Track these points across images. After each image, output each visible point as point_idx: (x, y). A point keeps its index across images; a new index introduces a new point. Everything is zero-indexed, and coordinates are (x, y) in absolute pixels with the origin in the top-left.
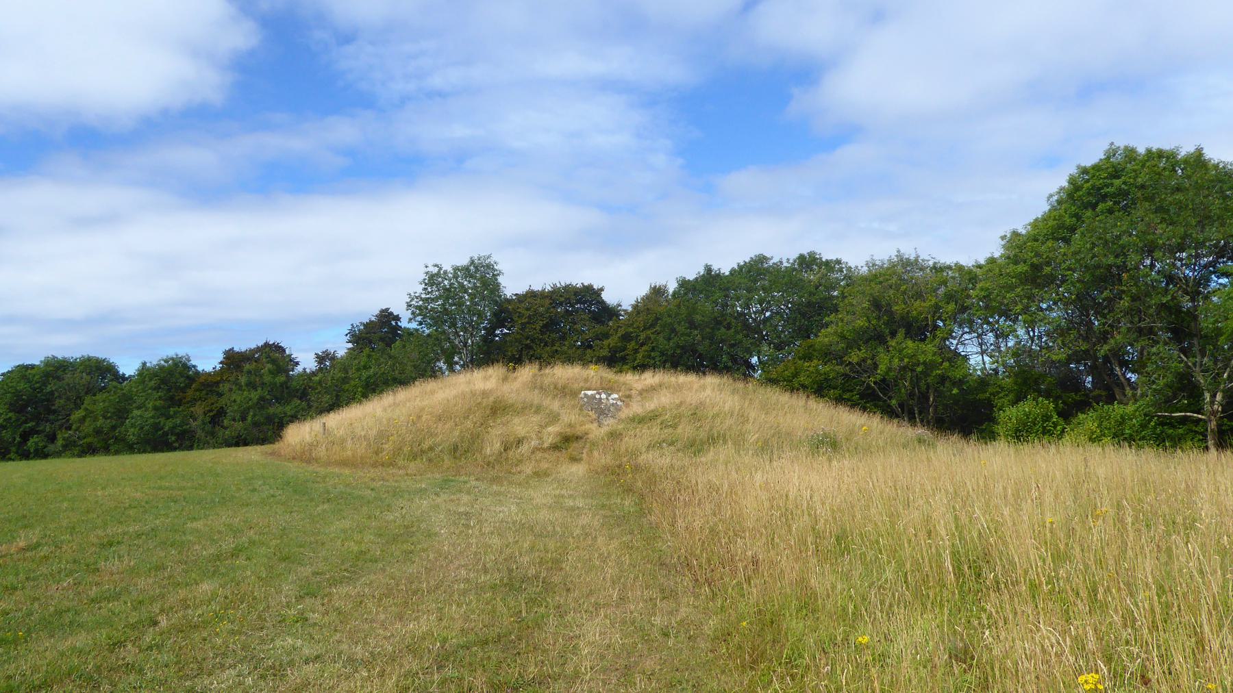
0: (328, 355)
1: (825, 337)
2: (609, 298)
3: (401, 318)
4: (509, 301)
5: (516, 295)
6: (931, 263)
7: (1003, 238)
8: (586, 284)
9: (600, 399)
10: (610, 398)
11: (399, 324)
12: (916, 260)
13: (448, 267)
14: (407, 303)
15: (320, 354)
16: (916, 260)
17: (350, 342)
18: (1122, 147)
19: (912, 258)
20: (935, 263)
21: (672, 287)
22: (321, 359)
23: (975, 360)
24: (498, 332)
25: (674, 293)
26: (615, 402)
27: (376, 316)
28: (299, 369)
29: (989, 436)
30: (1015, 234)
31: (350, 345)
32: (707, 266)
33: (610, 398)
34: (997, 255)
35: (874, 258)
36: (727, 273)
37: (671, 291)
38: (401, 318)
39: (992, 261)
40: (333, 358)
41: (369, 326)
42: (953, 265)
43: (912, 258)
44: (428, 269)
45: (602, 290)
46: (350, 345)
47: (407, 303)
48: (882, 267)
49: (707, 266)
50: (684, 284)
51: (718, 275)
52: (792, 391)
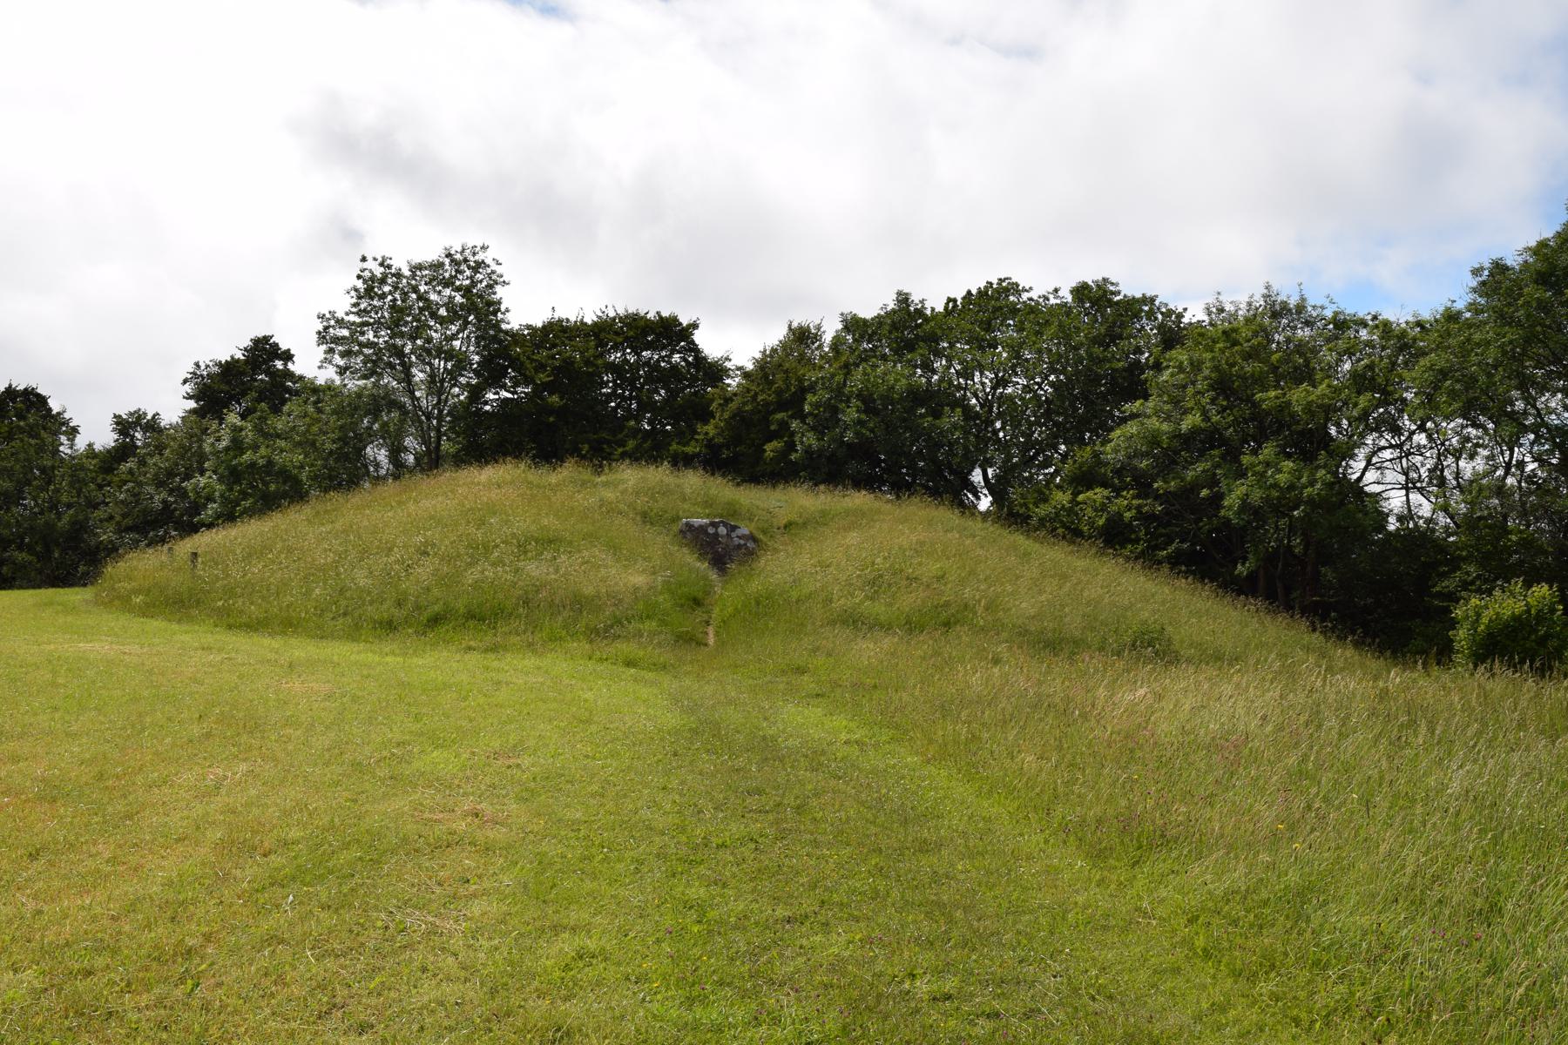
0: (139, 418)
1: (1119, 443)
2: (710, 343)
3: (293, 356)
4: (515, 336)
5: (529, 327)
6: (1329, 313)
7: (1476, 272)
8: (665, 314)
9: (716, 535)
10: (733, 535)
11: (290, 366)
12: (1301, 308)
13: (401, 263)
14: (319, 333)
15: (124, 417)
16: (1301, 308)
17: (189, 397)
18: (1487, 265)
19: (1293, 302)
20: (1336, 314)
21: (831, 330)
22: (124, 426)
23: (1395, 501)
24: (490, 396)
25: (837, 343)
26: (742, 542)
27: (246, 349)
28: (81, 443)
29: (1443, 653)
30: (1499, 268)
31: (192, 404)
32: (899, 293)
33: (733, 535)
34: (1460, 305)
35: (1221, 298)
36: (940, 308)
37: (828, 338)
38: (293, 356)
39: (1451, 316)
40: (152, 426)
41: (229, 370)
42: (1369, 317)
43: (1293, 302)
44: (365, 265)
45: (695, 326)
46: (192, 404)
47: (319, 333)
48: (1234, 315)
49: (899, 293)
50: (853, 324)
51: (920, 313)
52: (656, 461)
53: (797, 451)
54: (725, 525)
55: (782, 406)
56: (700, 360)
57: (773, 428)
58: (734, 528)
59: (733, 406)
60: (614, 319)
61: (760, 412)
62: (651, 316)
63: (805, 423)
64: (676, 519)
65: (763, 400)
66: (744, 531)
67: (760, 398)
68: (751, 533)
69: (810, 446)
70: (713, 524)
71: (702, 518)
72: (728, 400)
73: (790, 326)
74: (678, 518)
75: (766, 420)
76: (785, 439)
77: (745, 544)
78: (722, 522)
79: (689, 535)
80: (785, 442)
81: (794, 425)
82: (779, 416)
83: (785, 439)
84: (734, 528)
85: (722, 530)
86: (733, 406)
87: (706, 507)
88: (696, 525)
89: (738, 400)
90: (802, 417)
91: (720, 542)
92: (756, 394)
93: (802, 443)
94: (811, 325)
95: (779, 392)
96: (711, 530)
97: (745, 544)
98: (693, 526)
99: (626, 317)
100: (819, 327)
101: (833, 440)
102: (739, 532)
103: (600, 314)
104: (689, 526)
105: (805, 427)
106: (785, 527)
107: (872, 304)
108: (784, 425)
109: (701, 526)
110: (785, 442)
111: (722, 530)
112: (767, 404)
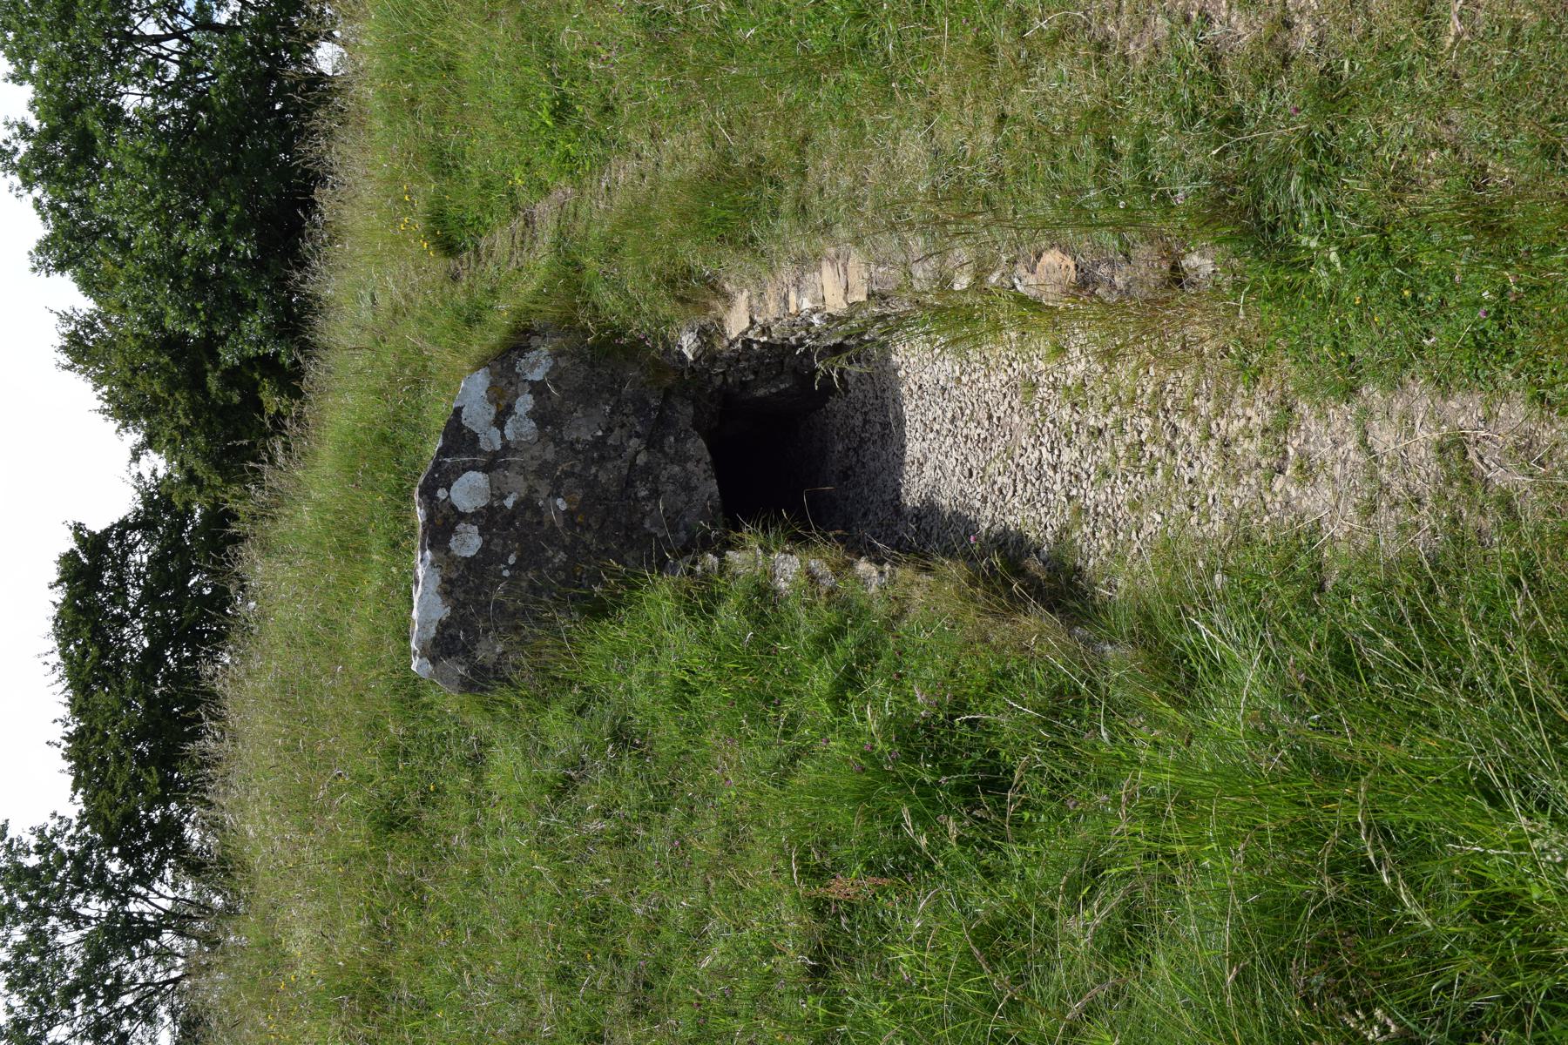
9: (488, 518)
10: (491, 440)
26: (525, 403)
33: (491, 440)
45: (78, 528)
53: (277, 354)
54: (442, 476)
55: (196, 382)
56: (144, 522)
57: (236, 399)
58: (458, 437)
59: (200, 468)
60: (63, 656)
61: (209, 422)
62: (59, 595)
63: (226, 337)
64: (409, 692)
65: (186, 415)
66: (473, 394)
67: (184, 421)
68: (482, 363)
69: (267, 328)
70: (441, 528)
71: (409, 579)
72: (191, 477)
73: (69, 368)
74: (409, 692)
75: (225, 412)
76: (257, 376)
77: (538, 389)
78: (428, 491)
79: (489, 650)
80: (263, 376)
81: (228, 357)
82: (213, 383)
83: (257, 376)
84: (458, 437)
85: (469, 491)
86: (200, 468)
87: (363, 550)
88: (441, 611)
89: (192, 462)
90: (210, 345)
91: (526, 503)
92: (178, 427)
93: (260, 343)
94: (64, 330)
95: (172, 385)
96: (468, 542)
97: (538, 389)
98: (443, 626)
99: (58, 636)
100: (66, 318)
101: (253, 281)
102: (478, 416)
103: (56, 677)
104: (443, 645)
105: (232, 337)
106: (449, 248)
107: (35, 212)
108: (231, 377)
109: (448, 589)
110: (263, 376)
111: (469, 491)
112: (195, 410)
